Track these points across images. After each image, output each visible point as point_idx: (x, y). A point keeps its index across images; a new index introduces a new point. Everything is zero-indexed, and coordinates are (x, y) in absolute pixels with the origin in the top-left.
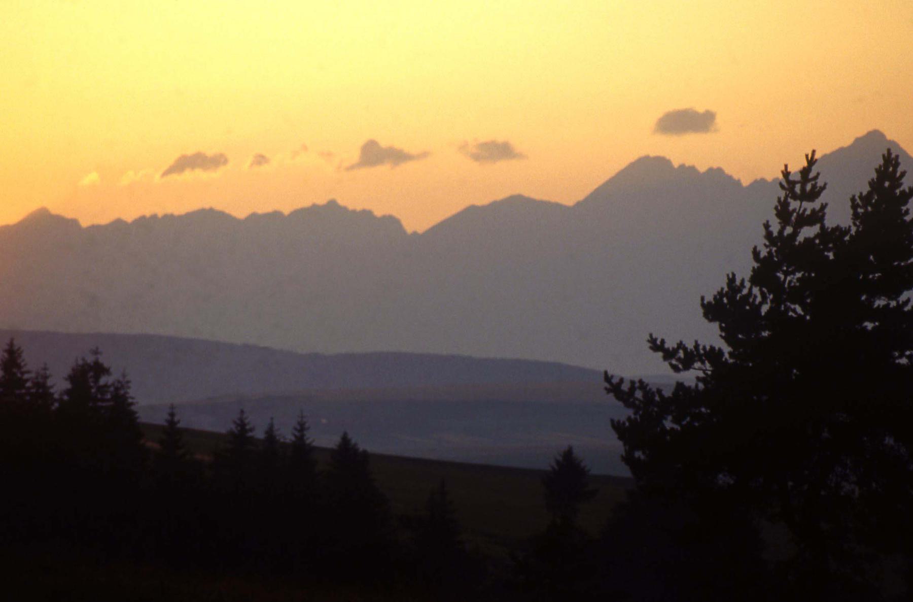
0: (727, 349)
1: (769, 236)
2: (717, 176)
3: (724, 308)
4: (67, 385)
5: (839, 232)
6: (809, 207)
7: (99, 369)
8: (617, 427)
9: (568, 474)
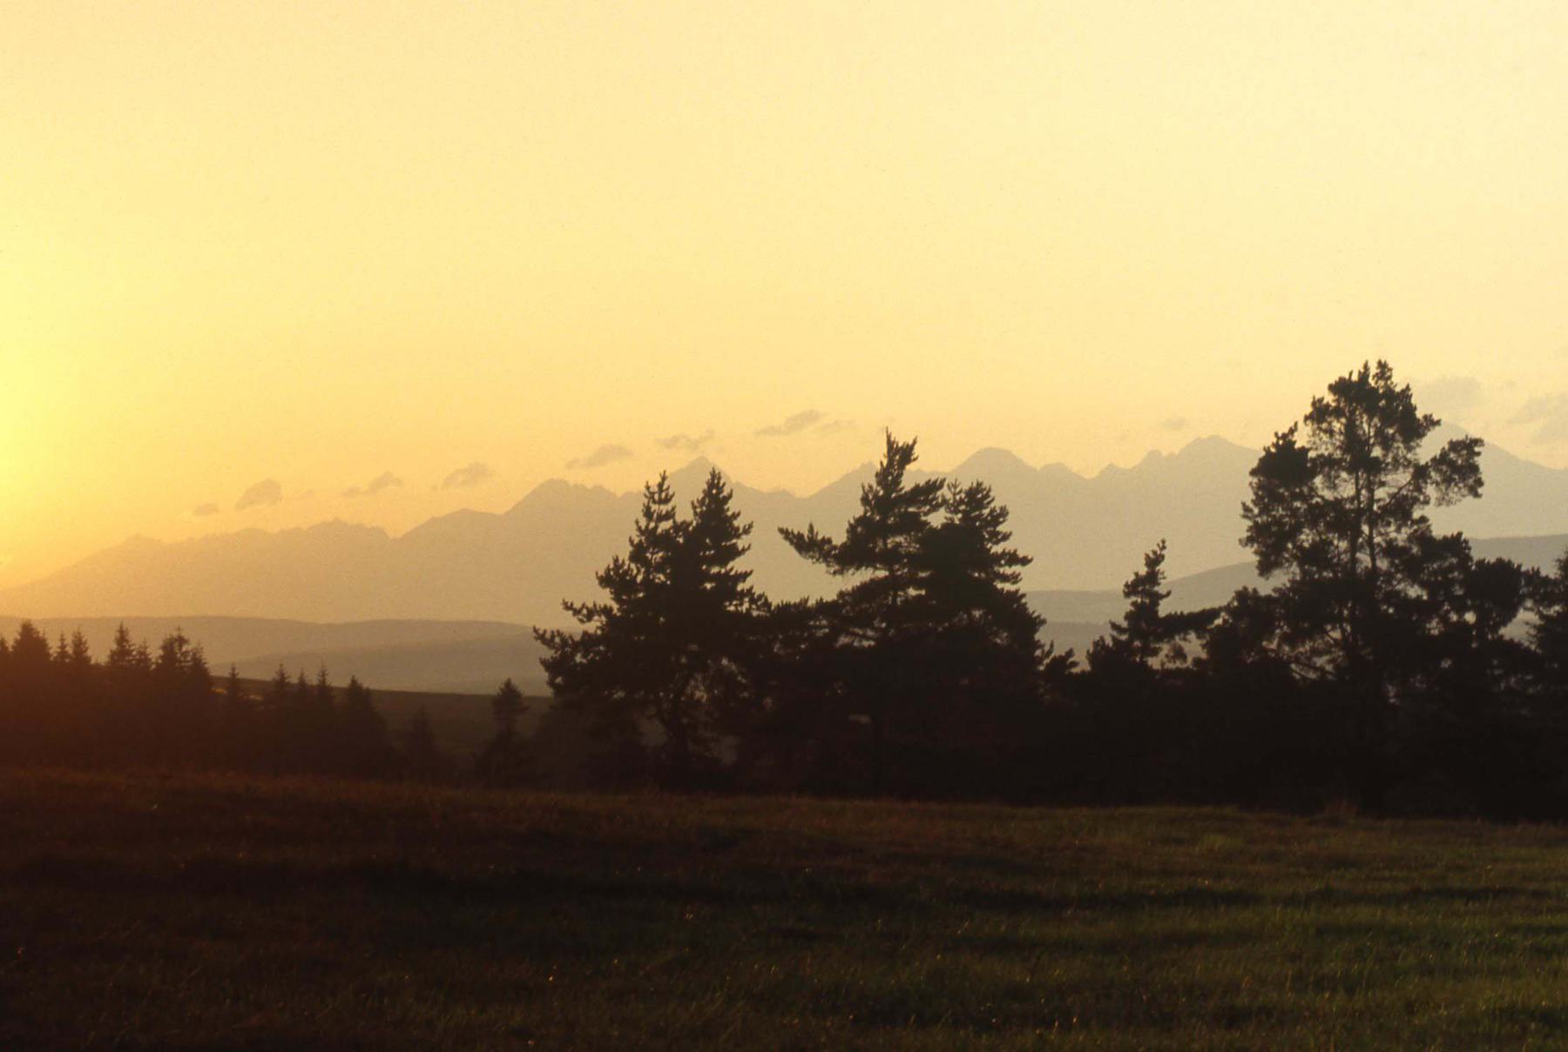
0: (615, 606)
1: (639, 529)
2: (599, 490)
3: (614, 579)
4: (161, 652)
5: (685, 525)
6: (664, 508)
7: (181, 641)
8: (544, 662)
9: (509, 698)
